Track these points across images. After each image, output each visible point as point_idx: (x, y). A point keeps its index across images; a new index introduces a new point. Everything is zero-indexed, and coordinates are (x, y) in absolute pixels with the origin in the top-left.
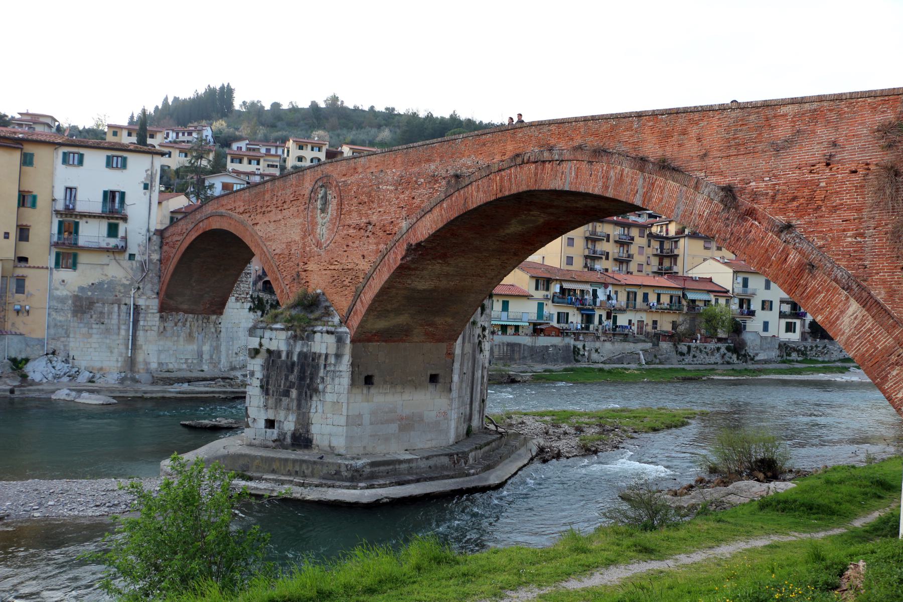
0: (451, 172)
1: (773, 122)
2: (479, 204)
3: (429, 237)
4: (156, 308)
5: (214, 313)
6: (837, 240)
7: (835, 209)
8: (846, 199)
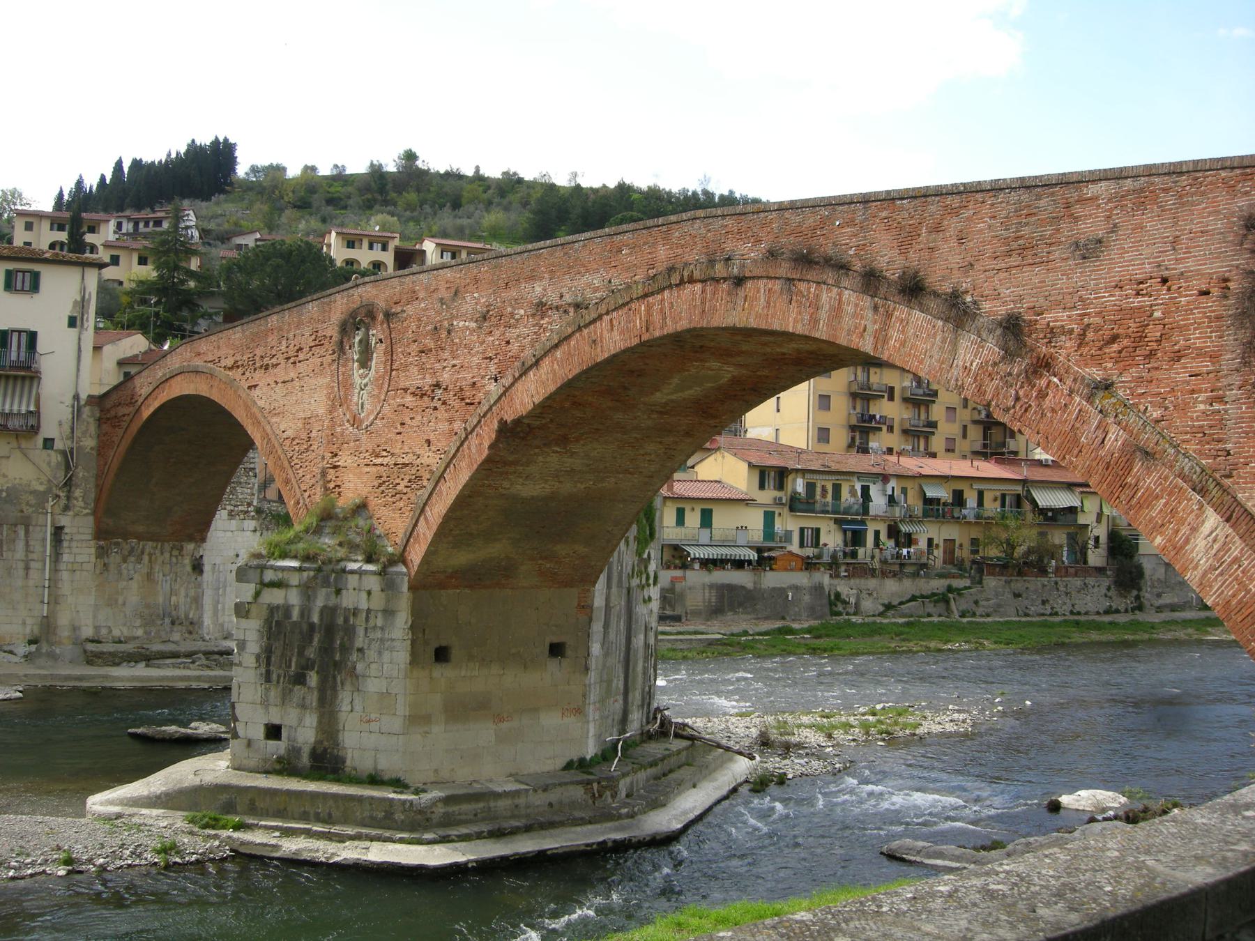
0: (568, 298)
1: (1077, 210)
2: (613, 352)
3: (533, 409)
4: (90, 531)
5: (191, 539)
6: (1182, 408)
7: (1177, 356)
8: (1195, 338)
